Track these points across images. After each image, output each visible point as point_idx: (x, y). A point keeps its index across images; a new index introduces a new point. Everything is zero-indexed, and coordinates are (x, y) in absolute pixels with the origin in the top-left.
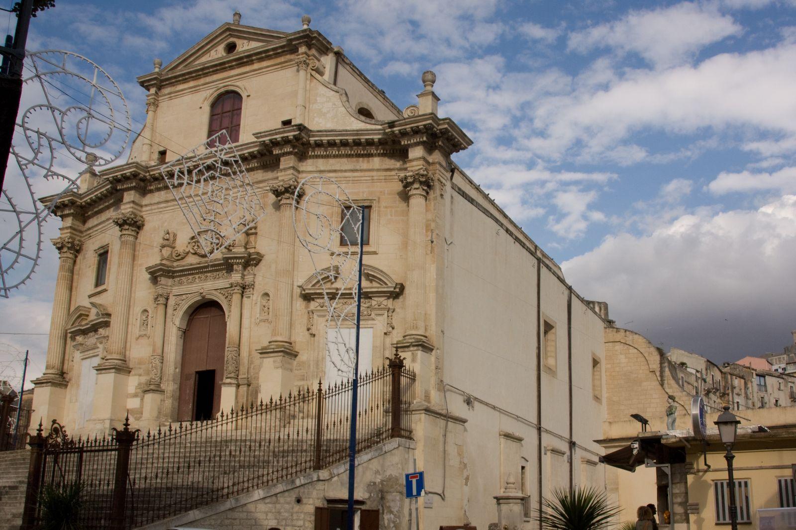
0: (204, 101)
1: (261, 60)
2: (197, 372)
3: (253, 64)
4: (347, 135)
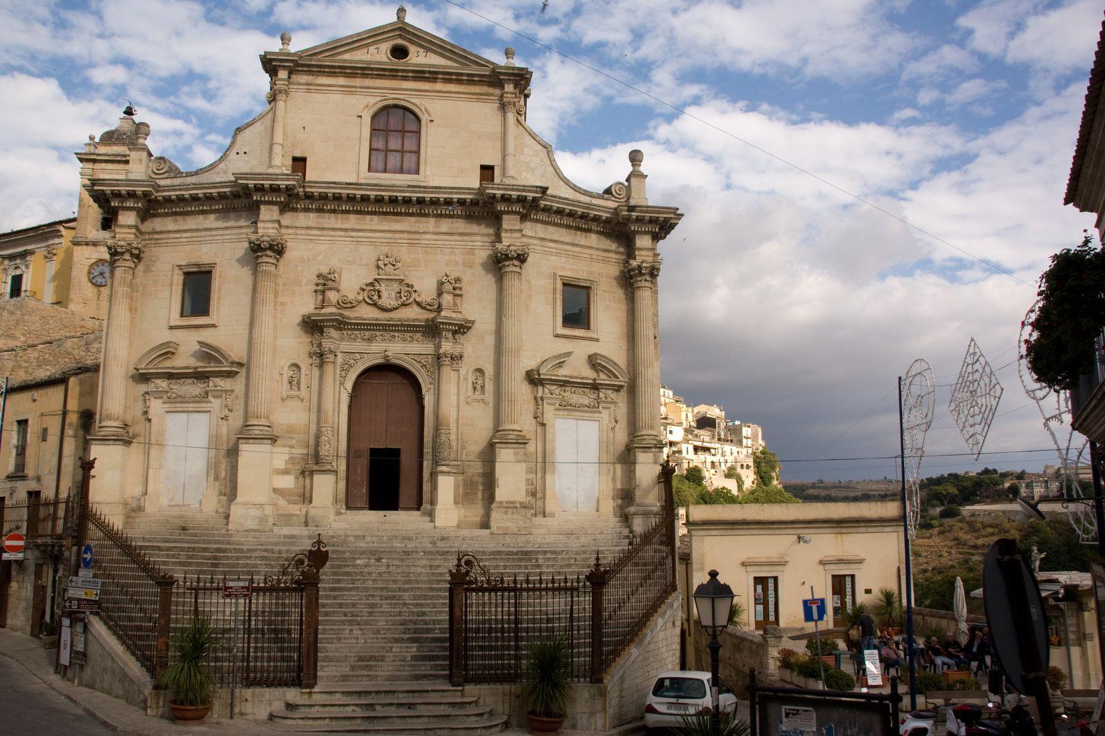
0: (364, 109)
2: (371, 449)
3: (436, 82)
4: (578, 206)
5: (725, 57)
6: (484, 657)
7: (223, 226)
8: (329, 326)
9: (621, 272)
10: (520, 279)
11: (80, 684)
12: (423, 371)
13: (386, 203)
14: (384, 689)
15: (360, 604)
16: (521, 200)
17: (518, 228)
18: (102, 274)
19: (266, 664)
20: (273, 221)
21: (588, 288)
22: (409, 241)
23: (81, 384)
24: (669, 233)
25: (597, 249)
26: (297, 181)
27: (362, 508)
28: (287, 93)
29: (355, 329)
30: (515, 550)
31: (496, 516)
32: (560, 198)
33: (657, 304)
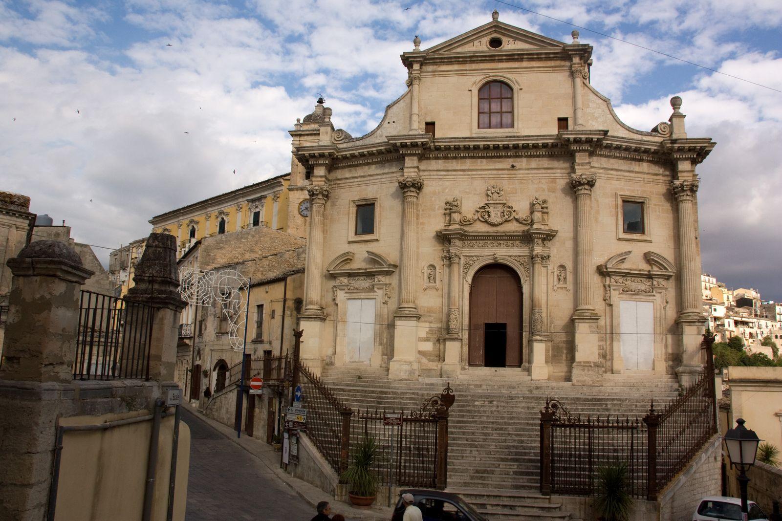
2: (486, 324)
3: (523, 61)
5: (756, 19)
6: (566, 475)
7: (381, 173)
8: (455, 238)
9: (668, 189)
10: (590, 199)
11: (295, 476)
12: (521, 268)
13: (491, 150)
14: (493, 494)
15: (477, 433)
16: (589, 141)
17: (587, 161)
19: (412, 471)
20: (414, 167)
21: (642, 203)
22: (508, 176)
23: (294, 281)
24: (705, 158)
25: (648, 174)
26: (429, 138)
28: (420, 79)
29: (472, 240)
30: (589, 397)
31: (576, 372)
32: (618, 137)
33: (697, 212)
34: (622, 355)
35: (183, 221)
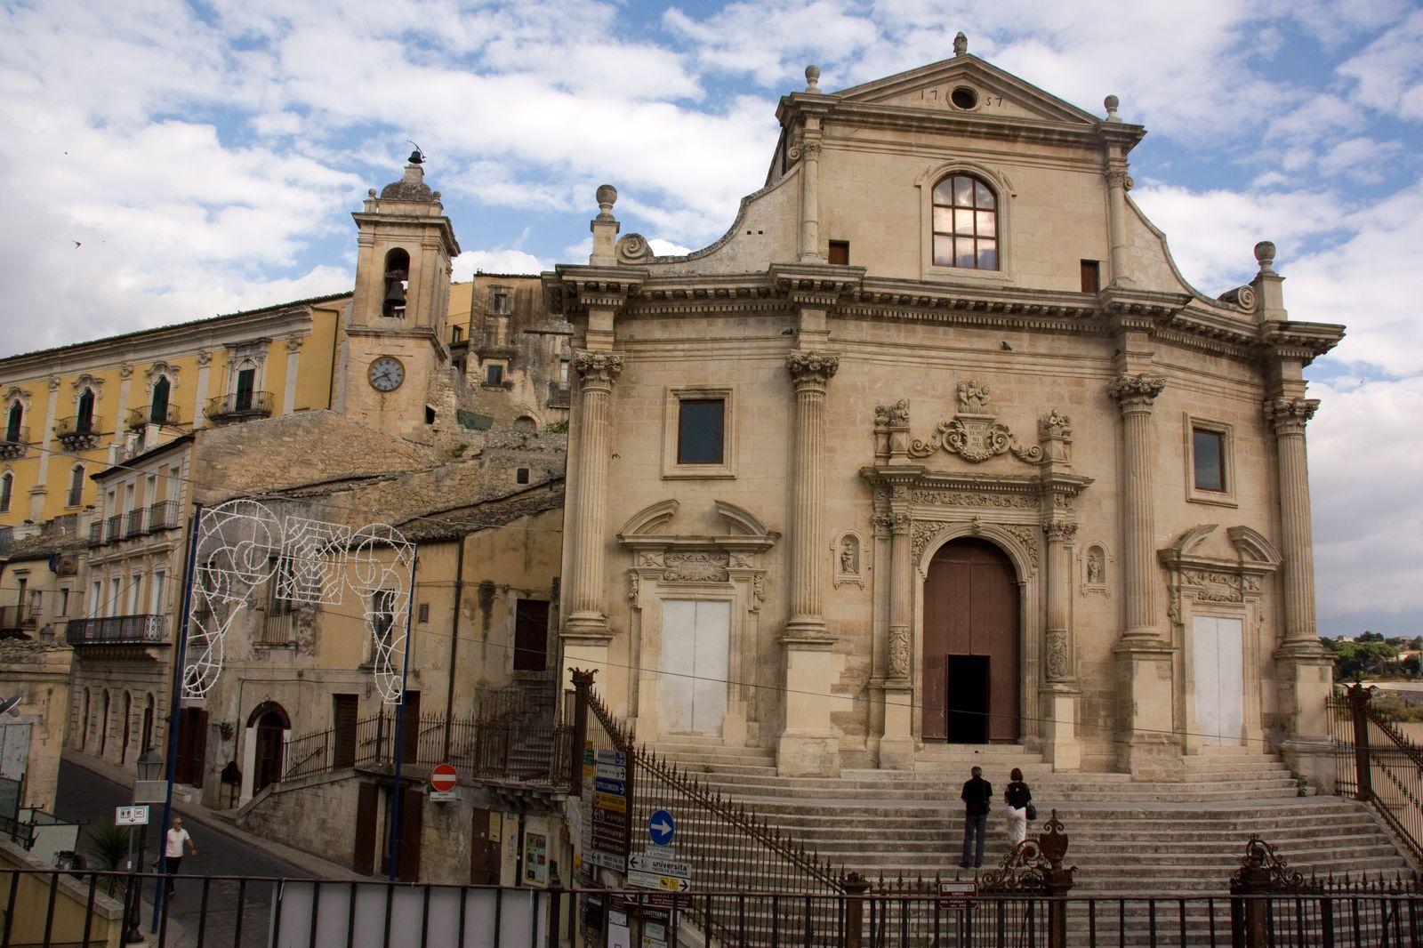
1: (1032, 140)
2: (950, 657)
3: (1015, 142)
13: (913, 307)
16: (1156, 312)
18: (386, 375)
20: (821, 333)
21: (1220, 435)
22: (998, 365)
25: (1231, 380)
27: (938, 741)
28: (819, 149)
31: (1138, 758)
34: (1197, 719)
35: (62, 376)
